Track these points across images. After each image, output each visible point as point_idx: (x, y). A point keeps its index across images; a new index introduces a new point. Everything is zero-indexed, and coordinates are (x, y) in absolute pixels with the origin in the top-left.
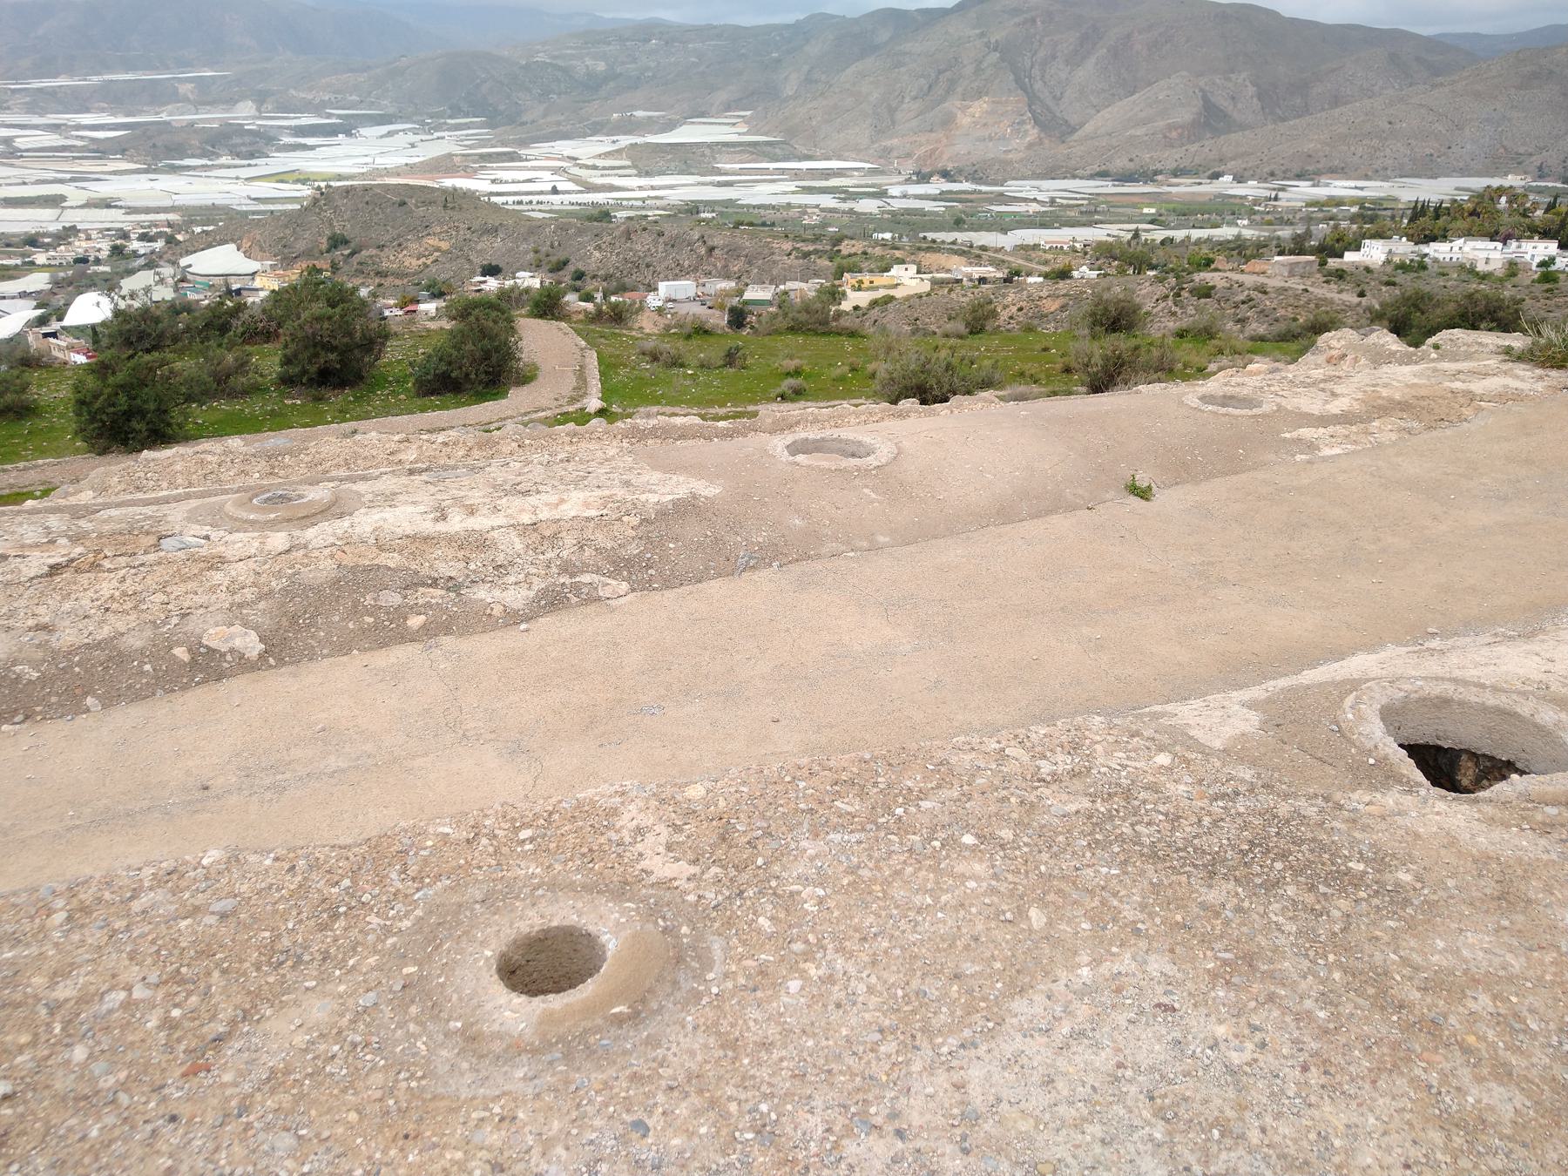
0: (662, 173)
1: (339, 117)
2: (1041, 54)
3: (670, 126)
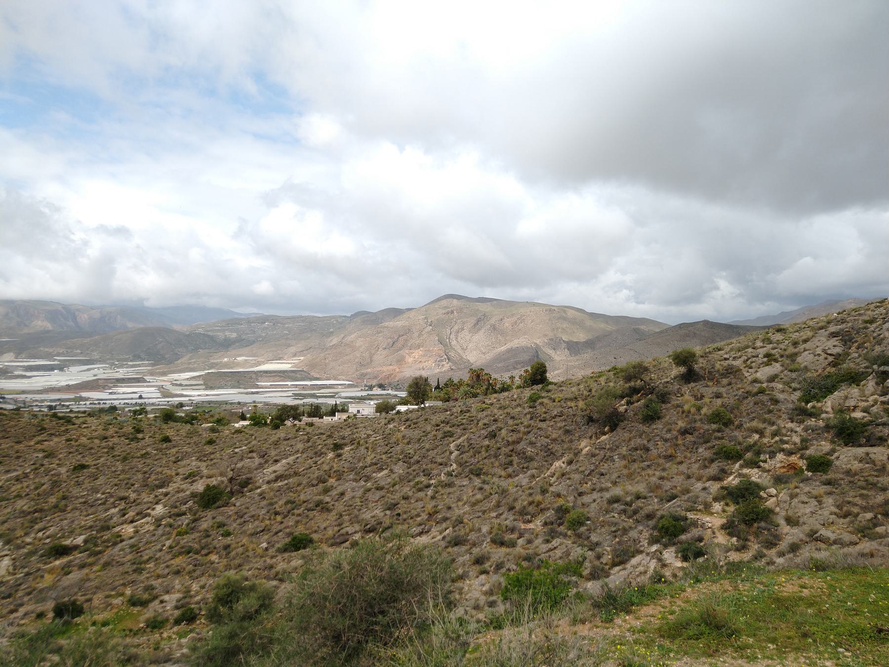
0: (222, 388)
1: (59, 360)
2: (456, 327)
3: (259, 364)
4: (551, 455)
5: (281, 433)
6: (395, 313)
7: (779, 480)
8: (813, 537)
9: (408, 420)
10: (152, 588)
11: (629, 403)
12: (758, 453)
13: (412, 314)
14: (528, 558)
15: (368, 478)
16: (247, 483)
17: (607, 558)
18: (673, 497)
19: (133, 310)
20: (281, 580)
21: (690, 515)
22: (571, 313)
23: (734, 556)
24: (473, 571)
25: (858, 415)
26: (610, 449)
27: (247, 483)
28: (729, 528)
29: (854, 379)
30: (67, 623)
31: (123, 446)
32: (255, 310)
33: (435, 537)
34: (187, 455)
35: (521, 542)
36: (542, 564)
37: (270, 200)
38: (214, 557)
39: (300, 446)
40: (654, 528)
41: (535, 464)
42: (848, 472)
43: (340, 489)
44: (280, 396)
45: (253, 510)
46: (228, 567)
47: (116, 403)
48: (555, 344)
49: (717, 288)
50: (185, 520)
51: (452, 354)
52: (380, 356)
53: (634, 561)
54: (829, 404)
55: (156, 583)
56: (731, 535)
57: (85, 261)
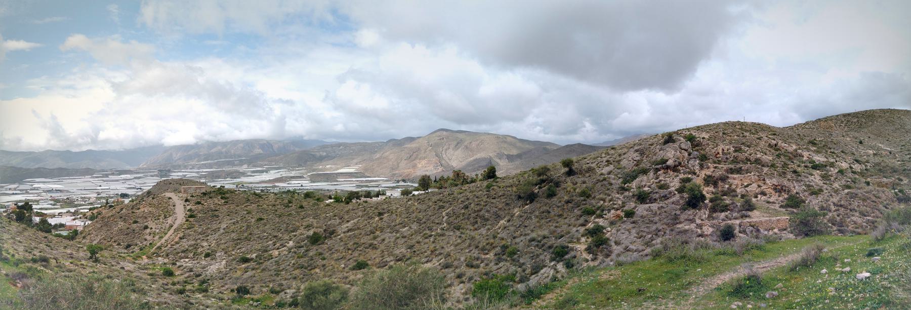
3: (338, 169)
4: (498, 217)
5: (350, 206)
6: (411, 139)
7: (612, 223)
8: (627, 249)
9: (418, 199)
10: (281, 285)
11: (540, 188)
12: (603, 211)
13: (420, 140)
14: (486, 274)
15: (397, 232)
16: (333, 232)
17: (528, 271)
18: (562, 236)
19: (297, 142)
20: (352, 285)
21: (570, 245)
22: (509, 139)
23: (591, 264)
24: (456, 282)
25: (646, 189)
26: (530, 213)
27: (333, 232)
28: (589, 250)
29: (645, 172)
30: (241, 297)
31: (281, 209)
32: (334, 140)
33: (435, 263)
34: (308, 216)
35: (482, 265)
36: (495, 276)
37: (341, 79)
38: (317, 270)
39: (360, 213)
40: (552, 253)
41: (490, 222)
42: (642, 217)
43: (382, 237)
44: (349, 186)
45: (336, 247)
46: (325, 276)
47: (290, 189)
48: (500, 156)
49: (584, 126)
50: (303, 250)
51: (443, 162)
52: (403, 164)
53: (542, 271)
54: (634, 184)
55: (284, 282)
56: (589, 253)
57: (274, 118)
